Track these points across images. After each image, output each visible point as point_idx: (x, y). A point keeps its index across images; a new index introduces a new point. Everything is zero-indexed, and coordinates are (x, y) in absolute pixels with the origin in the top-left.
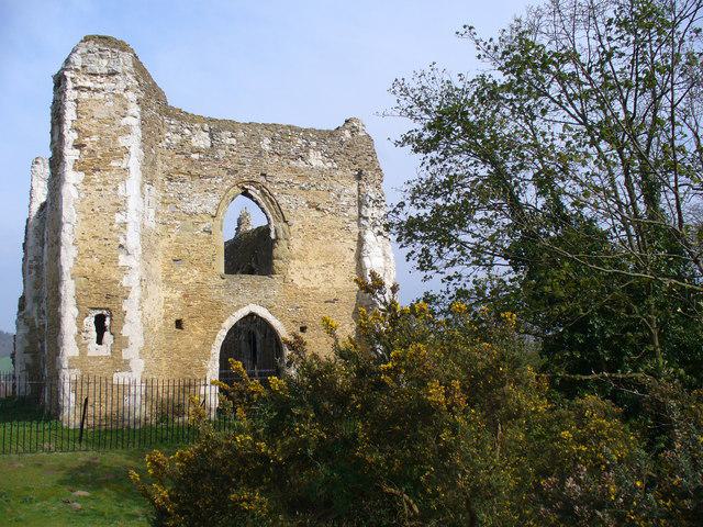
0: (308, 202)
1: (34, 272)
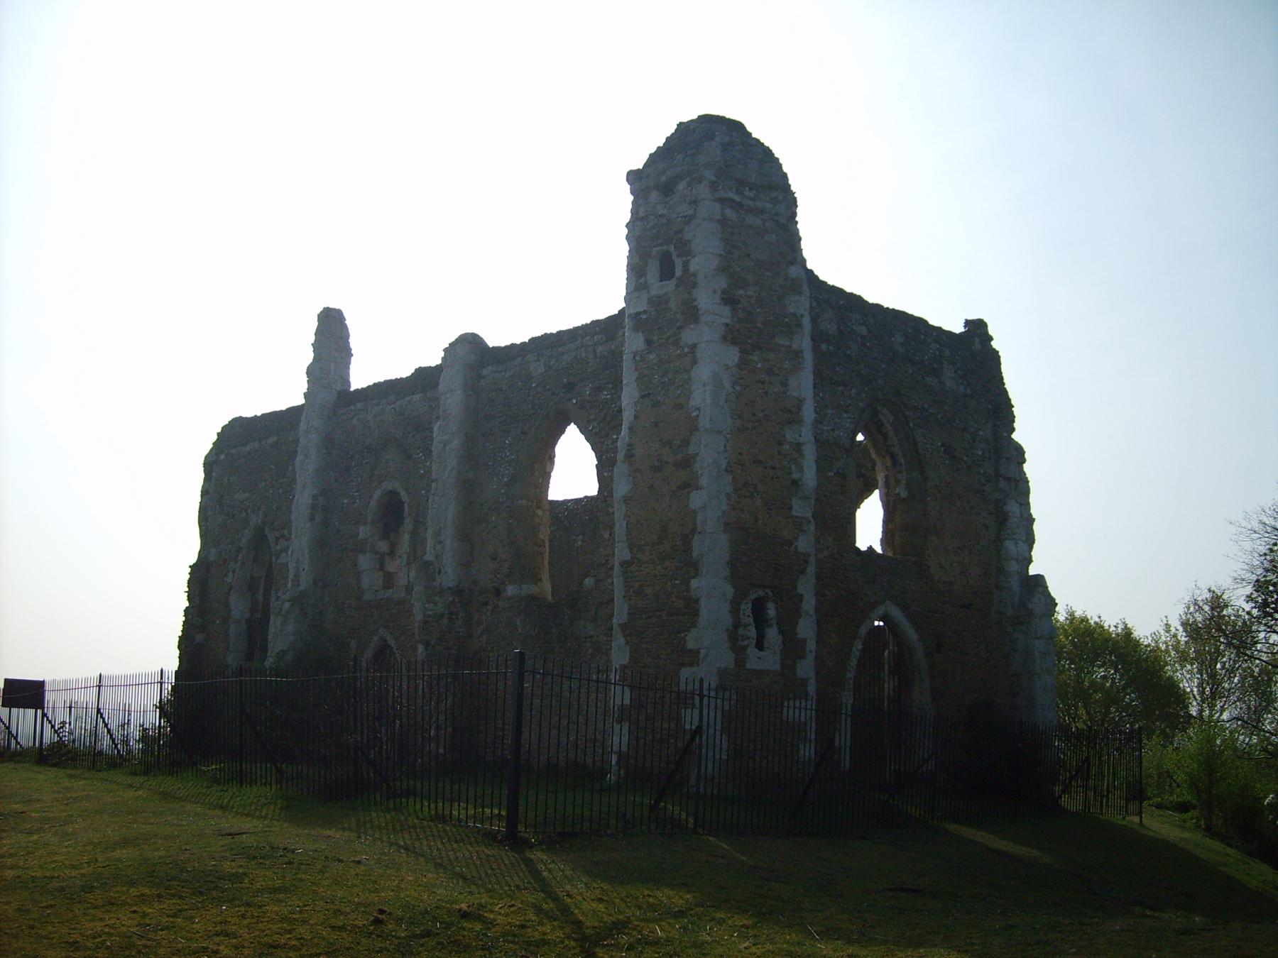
0: (943, 445)
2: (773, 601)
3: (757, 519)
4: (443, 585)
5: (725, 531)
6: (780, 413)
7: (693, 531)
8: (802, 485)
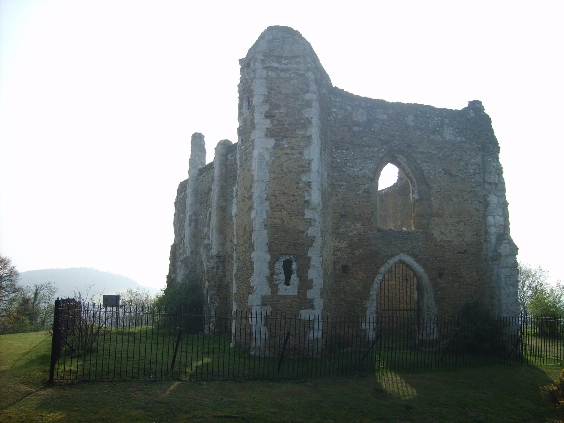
0: (443, 169)
1: (193, 224)
2: (295, 261)
3: (283, 222)
4: (212, 254)
5: (265, 229)
6: (298, 168)
7: (252, 231)
8: (311, 202)
